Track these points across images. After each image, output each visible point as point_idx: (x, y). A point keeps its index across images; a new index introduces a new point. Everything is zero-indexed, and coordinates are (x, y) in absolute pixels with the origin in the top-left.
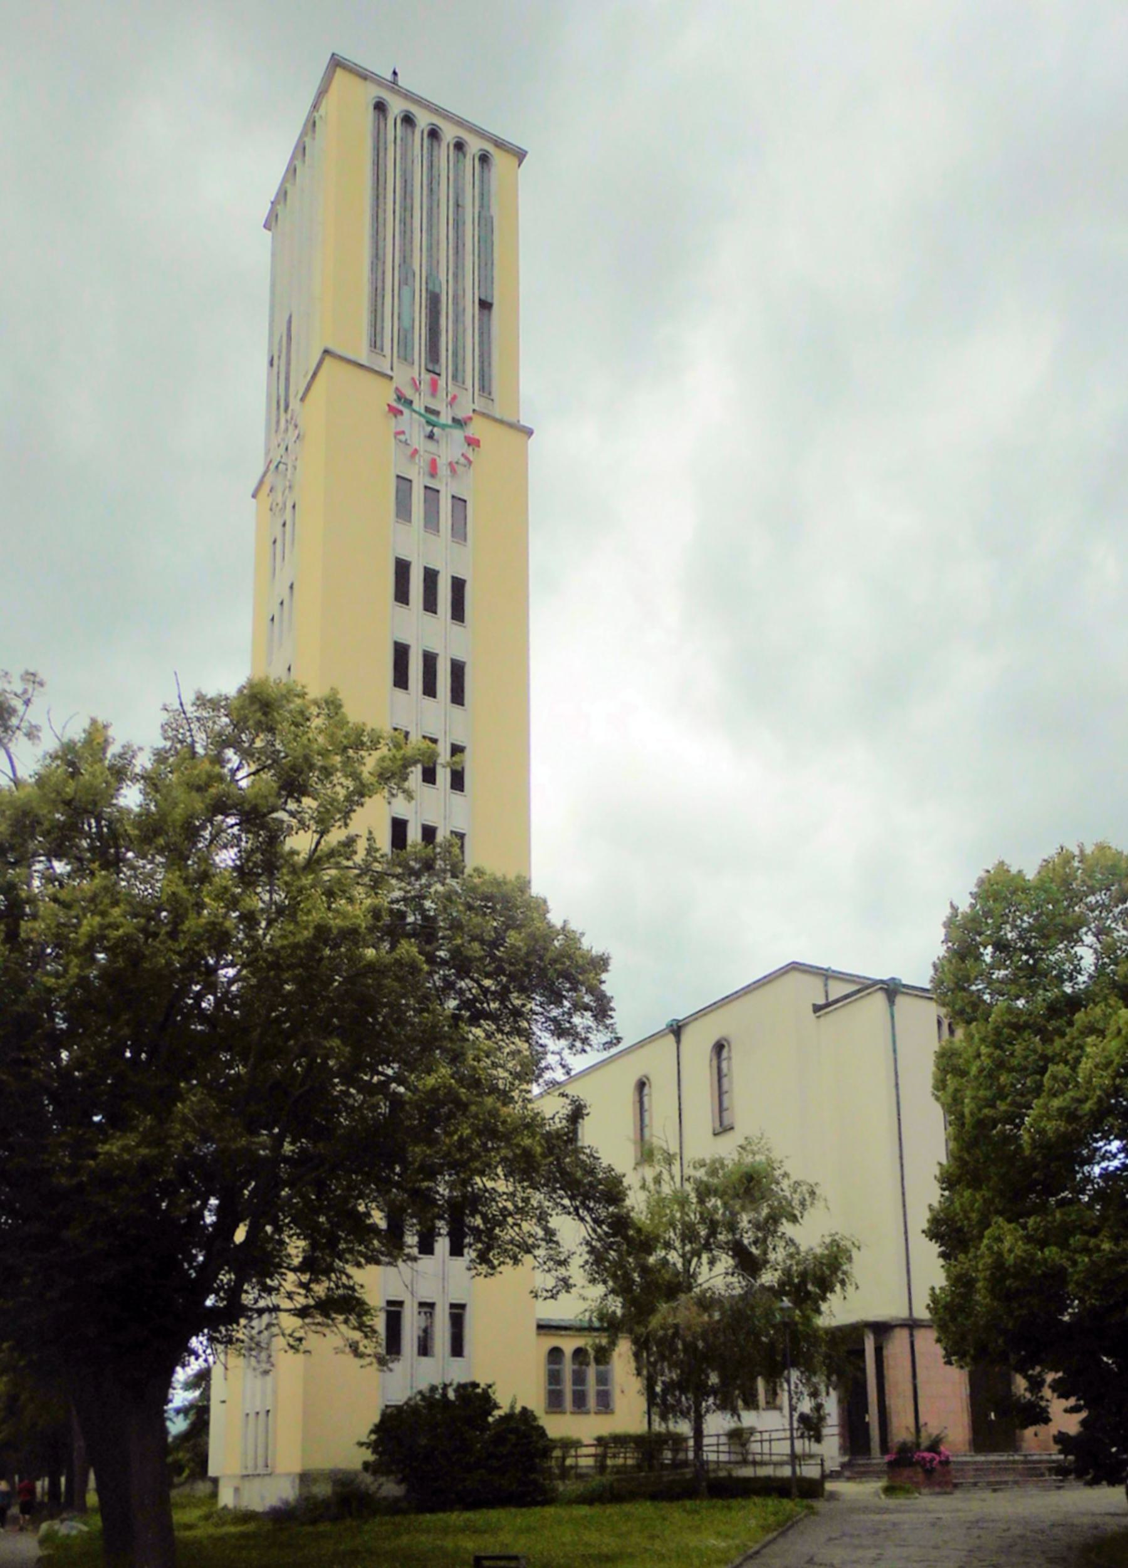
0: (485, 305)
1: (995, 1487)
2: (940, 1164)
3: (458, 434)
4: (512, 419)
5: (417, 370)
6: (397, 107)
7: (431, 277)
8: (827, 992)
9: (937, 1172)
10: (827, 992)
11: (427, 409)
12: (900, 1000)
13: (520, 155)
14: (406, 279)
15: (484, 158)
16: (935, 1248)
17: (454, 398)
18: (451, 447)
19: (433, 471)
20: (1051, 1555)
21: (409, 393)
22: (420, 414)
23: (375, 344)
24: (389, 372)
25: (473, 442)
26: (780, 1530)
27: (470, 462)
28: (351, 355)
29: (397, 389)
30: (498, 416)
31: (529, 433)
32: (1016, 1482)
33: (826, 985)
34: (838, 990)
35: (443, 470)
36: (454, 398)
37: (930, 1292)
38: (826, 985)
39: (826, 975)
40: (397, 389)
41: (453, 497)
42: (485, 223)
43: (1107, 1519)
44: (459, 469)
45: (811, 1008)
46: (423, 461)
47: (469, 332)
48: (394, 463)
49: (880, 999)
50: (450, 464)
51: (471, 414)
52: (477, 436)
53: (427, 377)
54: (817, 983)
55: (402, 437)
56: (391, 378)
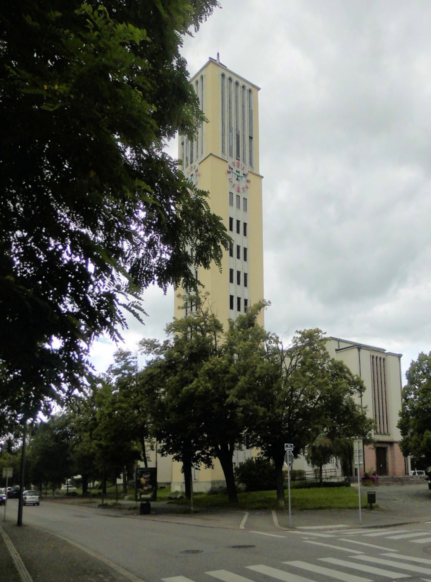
0: (251, 138)
1: (388, 485)
2: (400, 411)
3: (244, 179)
4: (257, 173)
5: (234, 159)
6: (227, 75)
7: (237, 129)
8: (339, 345)
9: (399, 412)
10: (339, 345)
11: (237, 171)
12: (362, 351)
13: (259, 89)
14: (231, 131)
15: (250, 91)
16: (399, 430)
17: (244, 168)
18: (243, 183)
19: (239, 191)
20: (377, 509)
21: (232, 166)
22: (235, 174)
23: (223, 151)
24: (227, 160)
25: (248, 181)
26: (170, 501)
27: (248, 187)
28: (218, 156)
29: (229, 166)
30: (254, 173)
31: (262, 177)
32: (392, 483)
33: (339, 343)
34: (342, 345)
35: (241, 190)
36: (244, 168)
37: (109, 366)
38: (339, 343)
39: (339, 341)
40: (229, 166)
41: (244, 198)
42: (251, 112)
43: (121, 571)
44: (245, 189)
45: (335, 350)
46: (236, 188)
47: (247, 146)
48: (228, 188)
49: (356, 350)
50: (243, 188)
51: (248, 173)
52: (250, 179)
53: (236, 161)
54: (336, 342)
55: (231, 180)
56: (227, 162)
